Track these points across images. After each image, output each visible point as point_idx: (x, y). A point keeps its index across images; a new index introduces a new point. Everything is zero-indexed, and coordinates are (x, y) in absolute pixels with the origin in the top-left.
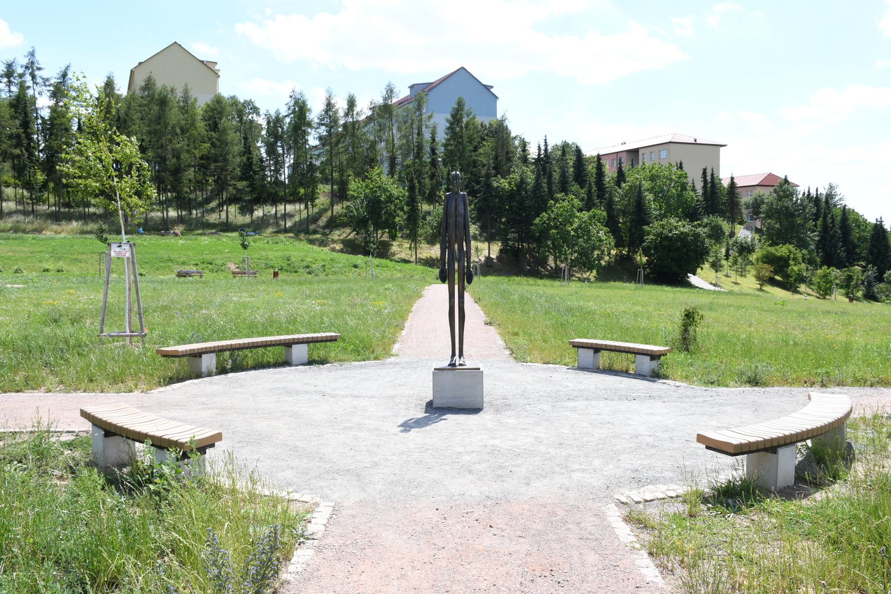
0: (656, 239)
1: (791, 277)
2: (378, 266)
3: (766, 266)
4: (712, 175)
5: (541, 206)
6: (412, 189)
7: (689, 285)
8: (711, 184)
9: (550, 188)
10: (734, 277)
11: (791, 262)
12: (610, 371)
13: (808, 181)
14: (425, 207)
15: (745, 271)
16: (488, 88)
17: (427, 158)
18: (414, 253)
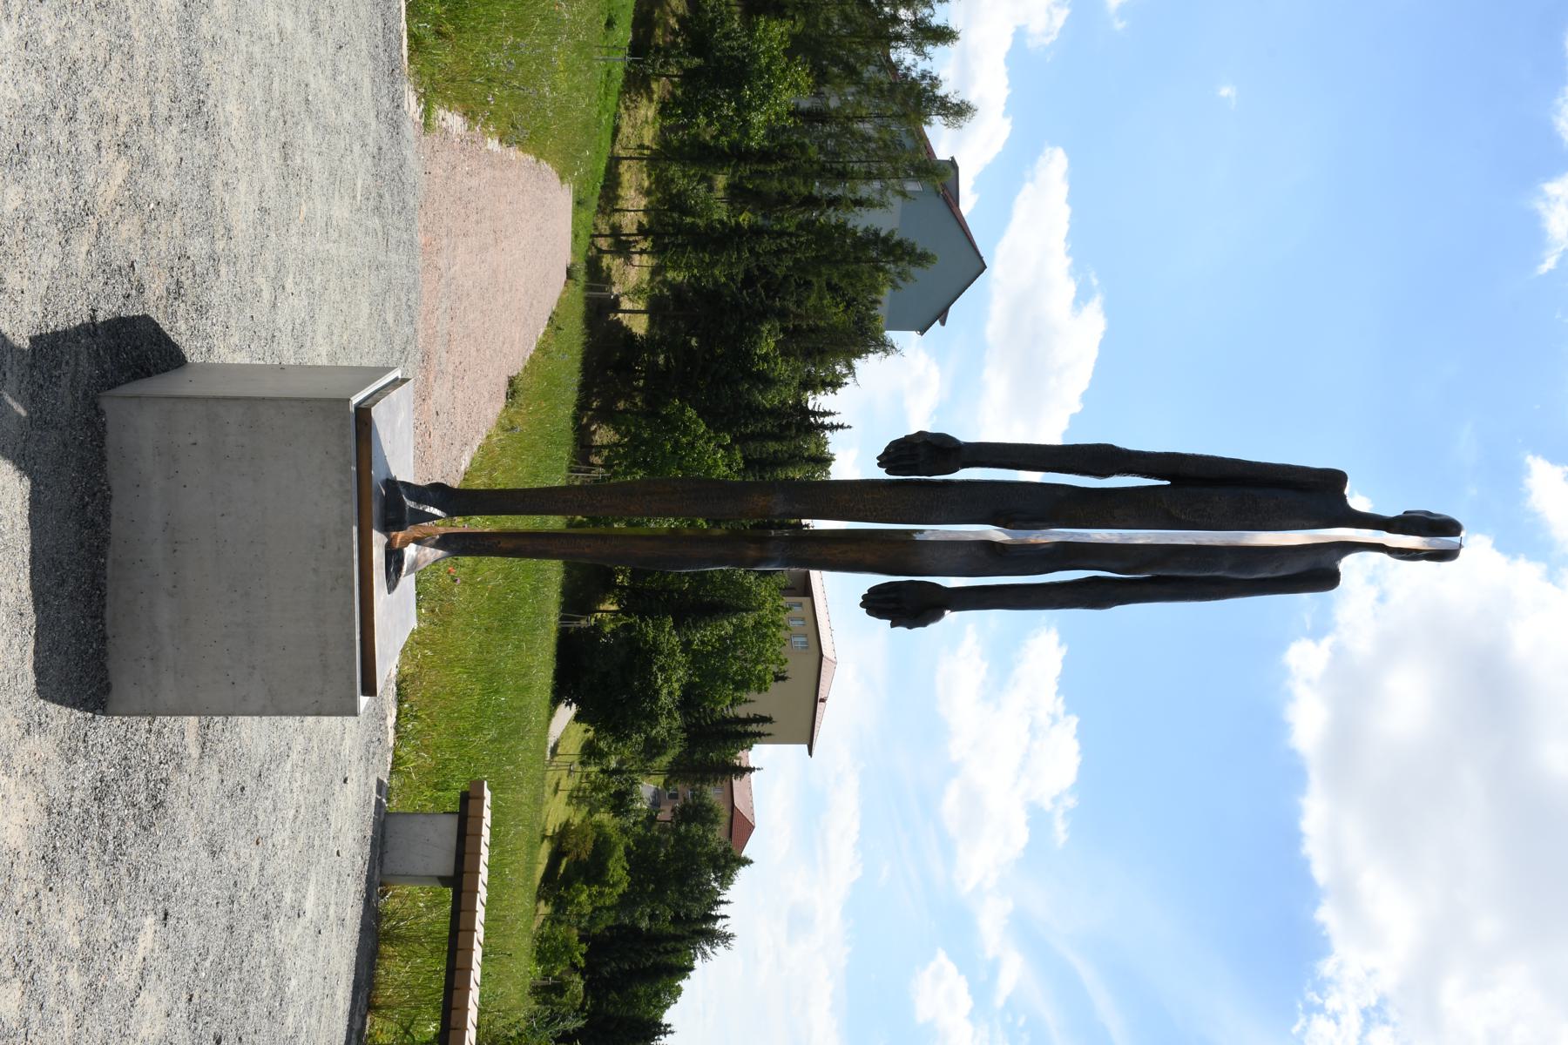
0: (646, 642)
1: (567, 889)
2: (609, 73)
3: (590, 845)
4: (760, 735)
5: (716, 418)
6: (764, 156)
7: (555, 703)
8: (746, 732)
9: (753, 437)
10: (567, 784)
11: (595, 889)
12: (375, 936)
13: (740, 903)
14: (721, 181)
15: (579, 804)
16: (942, 316)
17: (817, 188)
18: (630, 153)
